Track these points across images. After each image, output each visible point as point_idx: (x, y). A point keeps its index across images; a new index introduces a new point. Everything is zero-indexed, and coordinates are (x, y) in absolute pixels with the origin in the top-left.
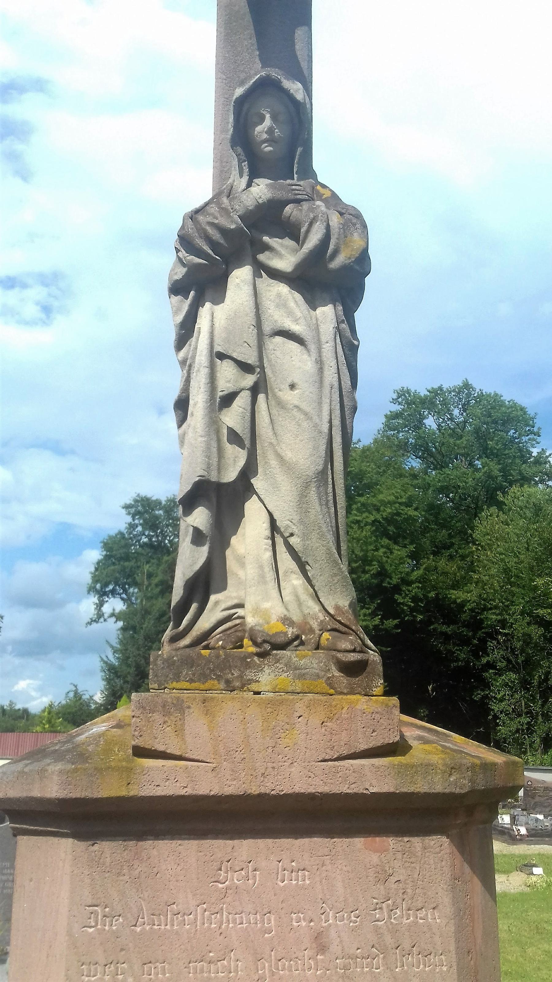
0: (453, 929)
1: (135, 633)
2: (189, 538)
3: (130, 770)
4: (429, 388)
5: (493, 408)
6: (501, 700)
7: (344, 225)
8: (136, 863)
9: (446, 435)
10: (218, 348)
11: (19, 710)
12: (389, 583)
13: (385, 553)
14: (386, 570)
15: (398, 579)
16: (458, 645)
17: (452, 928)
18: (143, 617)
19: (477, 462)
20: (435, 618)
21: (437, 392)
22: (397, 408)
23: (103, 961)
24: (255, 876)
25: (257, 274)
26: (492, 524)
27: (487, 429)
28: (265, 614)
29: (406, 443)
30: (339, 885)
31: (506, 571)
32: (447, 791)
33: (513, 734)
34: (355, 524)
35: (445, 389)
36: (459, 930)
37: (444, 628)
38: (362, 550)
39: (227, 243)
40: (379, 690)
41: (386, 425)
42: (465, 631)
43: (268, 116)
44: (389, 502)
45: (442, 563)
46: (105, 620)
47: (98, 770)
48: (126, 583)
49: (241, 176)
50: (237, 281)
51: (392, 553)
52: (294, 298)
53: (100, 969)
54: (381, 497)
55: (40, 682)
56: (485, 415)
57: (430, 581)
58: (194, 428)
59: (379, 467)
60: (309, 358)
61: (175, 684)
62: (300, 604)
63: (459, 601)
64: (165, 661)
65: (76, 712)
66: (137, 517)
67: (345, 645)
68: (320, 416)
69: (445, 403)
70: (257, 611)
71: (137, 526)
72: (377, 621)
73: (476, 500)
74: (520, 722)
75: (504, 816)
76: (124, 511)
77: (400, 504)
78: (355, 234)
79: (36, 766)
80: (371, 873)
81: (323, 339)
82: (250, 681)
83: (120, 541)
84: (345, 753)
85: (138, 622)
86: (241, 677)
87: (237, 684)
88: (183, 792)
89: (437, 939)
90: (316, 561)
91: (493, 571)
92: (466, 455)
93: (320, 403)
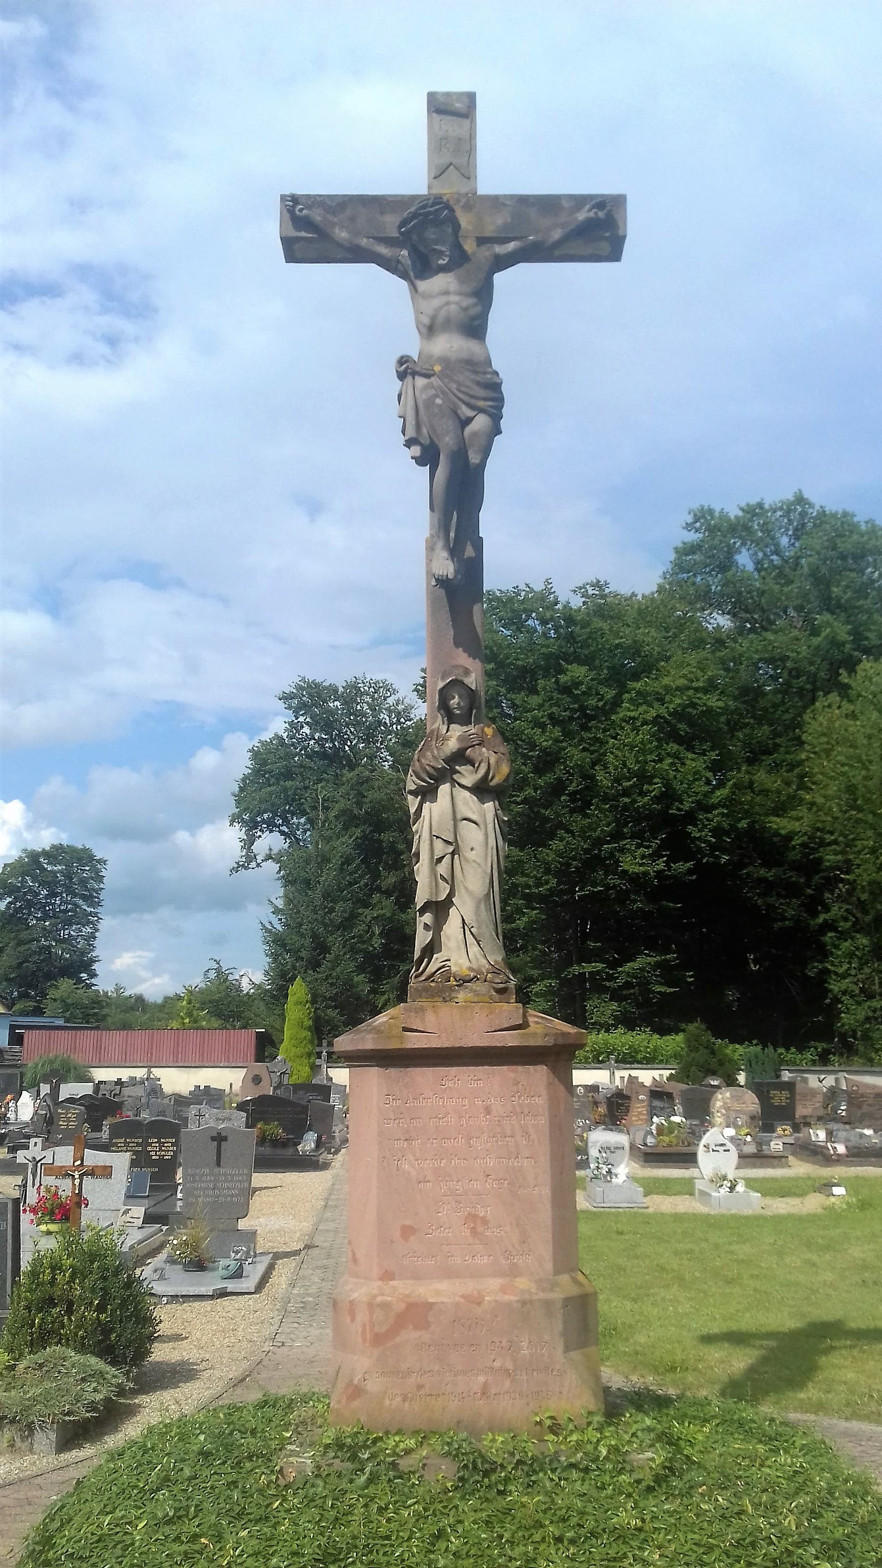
4: (743, 505)
5: (840, 536)
6: (844, 976)
11: (130, 997)
12: (679, 810)
13: (673, 764)
14: (674, 789)
15: (693, 803)
16: (785, 897)
17: (547, 1105)
18: (320, 866)
21: (754, 511)
22: (692, 537)
25: (453, 786)
28: (460, 966)
31: (851, 789)
34: (628, 722)
35: (767, 507)
37: (762, 872)
38: (637, 762)
40: (512, 1001)
41: (676, 565)
42: (794, 876)
44: (678, 689)
45: (761, 776)
46: (258, 865)
47: (389, 1037)
48: (289, 811)
49: (443, 723)
51: (683, 764)
54: (666, 681)
56: (827, 548)
57: (742, 803)
59: (667, 630)
62: (477, 960)
65: (221, 1000)
68: (486, 864)
69: (766, 529)
70: (456, 964)
71: (302, 727)
72: (661, 865)
73: (813, 679)
75: (819, 1132)
76: (281, 705)
77: (696, 690)
81: (488, 822)
82: (454, 998)
86: (449, 996)
87: (448, 999)
91: (832, 790)
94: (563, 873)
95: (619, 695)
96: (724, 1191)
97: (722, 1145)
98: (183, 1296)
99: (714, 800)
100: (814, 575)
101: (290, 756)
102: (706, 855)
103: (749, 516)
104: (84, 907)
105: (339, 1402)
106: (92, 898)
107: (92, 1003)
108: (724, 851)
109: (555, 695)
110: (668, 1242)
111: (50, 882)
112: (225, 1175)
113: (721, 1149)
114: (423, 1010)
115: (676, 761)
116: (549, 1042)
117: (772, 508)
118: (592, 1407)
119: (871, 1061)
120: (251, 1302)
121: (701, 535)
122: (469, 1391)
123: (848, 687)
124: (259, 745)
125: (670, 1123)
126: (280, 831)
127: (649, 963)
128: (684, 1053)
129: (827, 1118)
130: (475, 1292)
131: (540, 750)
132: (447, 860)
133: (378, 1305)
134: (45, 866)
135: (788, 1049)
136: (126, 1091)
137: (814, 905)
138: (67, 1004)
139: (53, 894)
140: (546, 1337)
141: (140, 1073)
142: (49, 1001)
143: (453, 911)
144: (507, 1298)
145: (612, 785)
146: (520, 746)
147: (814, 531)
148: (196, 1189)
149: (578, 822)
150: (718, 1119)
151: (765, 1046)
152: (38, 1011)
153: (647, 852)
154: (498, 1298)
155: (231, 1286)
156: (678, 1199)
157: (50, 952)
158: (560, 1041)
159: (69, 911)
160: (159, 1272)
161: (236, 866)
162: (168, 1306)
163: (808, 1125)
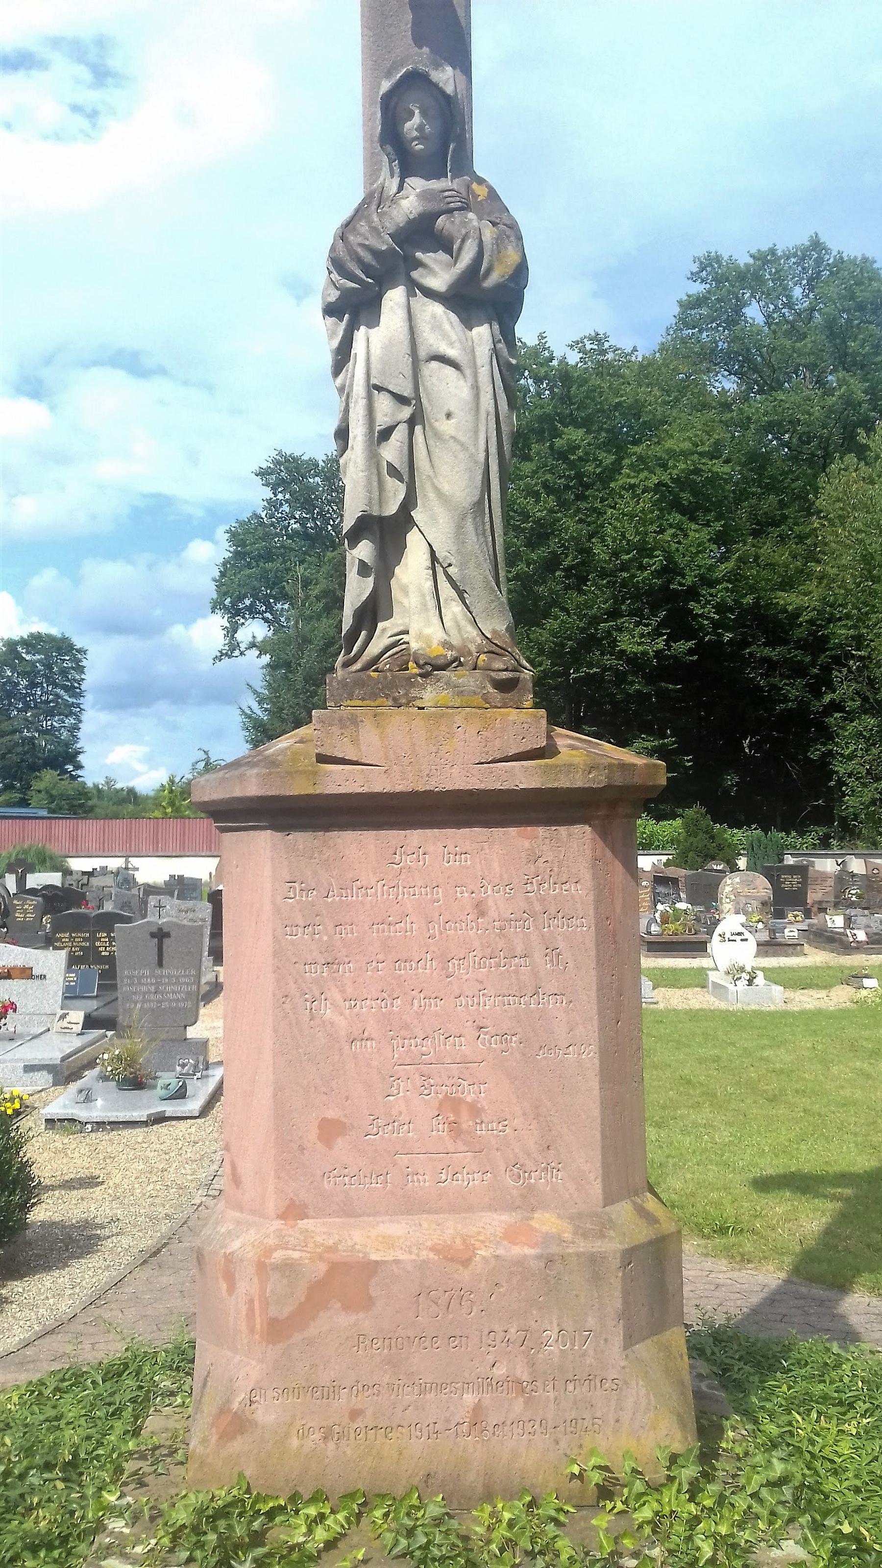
0: (592, 898)
1: (290, 672)
2: (355, 569)
3: (315, 773)
5: (858, 283)
6: (851, 757)
7: (497, 239)
8: (325, 849)
9: (779, 334)
10: (374, 381)
11: (122, 789)
12: (681, 584)
13: (674, 536)
14: (676, 563)
16: (788, 678)
17: (591, 898)
19: (830, 378)
20: (753, 636)
21: (766, 258)
22: (698, 288)
23: (302, 924)
24: (424, 859)
25: (411, 294)
26: (847, 483)
27: (849, 321)
28: (428, 639)
29: (713, 350)
30: (496, 865)
32: (586, 786)
33: (867, 807)
34: (627, 490)
35: (779, 253)
36: (598, 901)
37: (767, 651)
38: (638, 533)
39: (378, 262)
40: (528, 704)
42: (798, 655)
43: (417, 112)
45: (767, 549)
46: (242, 654)
47: (289, 773)
48: (271, 596)
49: (392, 176)
50: (391, 303)
51: (686, 535)
52: (449, 319)
53: (300, 930)
54: (669, 444)
55: (146, 749)
56: (844, 297)
58: (355, 462)
60: (464, 384)
61: (349, 702)
62: (459, 629)
63: (790, 608)
64: (339, 682)
66: (280, 490)
67: (499, 665)
68: (476, 445)
70: (419, 636)
71: (281, 504)
72: (660, 643)
74: (876, 789)
75: (834, 918)
77: (701, 454)
78: (510, 248)
79: (237, 773)
80: (523, 855)
81: (479, 362)
83: (256, 529)
84: (498, 757)
85: (293, 655)
86: (406, 694)
87: (404, 701)
88: (360, 790)
89: (578, 905)
90: (473, 589)
92: (811, 367)
93: (476, 432)
94: (556, 654)
95: (619, 460)
96: (742, 984)
97: (739, 934)
98: (110, 1123)
99: (718, 574)
100: (830, 327)
101: (267, 537)
102: (708, 633)
103: (759, 263)
104: (67, 698)
105: (204, 1441)
106: (74, 690)
107: (79, 794)
108: (728, 629)
109: (550, 461)
110: (689, 1046)
111: (30, 673)
112: (169, 977)
113: (738, 938)
114: (354, 721)
115: (678, 532)
116: (597, 780)
117: (784, 254)
118: (677, 1447)
119: (875, 844)
120: (193, 1129)
121: (708, 286)
122: (448, 1421)
123: (866, 447)
124: (236, 525)
125: (675, 910)
126: (263, 619)
127: (646, 748)
128: (681, 838)
129: (840, 903)
130: (458, 1241)
131: (534, 522)
132: (399, 435)
133: (276, 1267)
134: (24, 655)
135: (788, 834)
136: (94, 881)
137: (824, 682)
138: (51, 796)
139: (33, 685)
140: (591, 1322)
141: (115, 864)
142: (33, 793)
143: (413, 538)
144: (518, 1251)
145: (610, 559)
146: (512, 518)
147: (831, 279)
148: (135, 993)
149: (574, 599)
150: (727, 906)
151: (766, 830)
152: (24, 803)
153: (646, 630)
154: (501, 1252)
155: (170, 1108)
156: (689, 992)
157: (33, 744)
158: (618, 780)
159: (50, 702)
160: (84, 1093)
161: (219, 654)
162: (93, 1135)
163: (823, 910)
